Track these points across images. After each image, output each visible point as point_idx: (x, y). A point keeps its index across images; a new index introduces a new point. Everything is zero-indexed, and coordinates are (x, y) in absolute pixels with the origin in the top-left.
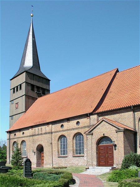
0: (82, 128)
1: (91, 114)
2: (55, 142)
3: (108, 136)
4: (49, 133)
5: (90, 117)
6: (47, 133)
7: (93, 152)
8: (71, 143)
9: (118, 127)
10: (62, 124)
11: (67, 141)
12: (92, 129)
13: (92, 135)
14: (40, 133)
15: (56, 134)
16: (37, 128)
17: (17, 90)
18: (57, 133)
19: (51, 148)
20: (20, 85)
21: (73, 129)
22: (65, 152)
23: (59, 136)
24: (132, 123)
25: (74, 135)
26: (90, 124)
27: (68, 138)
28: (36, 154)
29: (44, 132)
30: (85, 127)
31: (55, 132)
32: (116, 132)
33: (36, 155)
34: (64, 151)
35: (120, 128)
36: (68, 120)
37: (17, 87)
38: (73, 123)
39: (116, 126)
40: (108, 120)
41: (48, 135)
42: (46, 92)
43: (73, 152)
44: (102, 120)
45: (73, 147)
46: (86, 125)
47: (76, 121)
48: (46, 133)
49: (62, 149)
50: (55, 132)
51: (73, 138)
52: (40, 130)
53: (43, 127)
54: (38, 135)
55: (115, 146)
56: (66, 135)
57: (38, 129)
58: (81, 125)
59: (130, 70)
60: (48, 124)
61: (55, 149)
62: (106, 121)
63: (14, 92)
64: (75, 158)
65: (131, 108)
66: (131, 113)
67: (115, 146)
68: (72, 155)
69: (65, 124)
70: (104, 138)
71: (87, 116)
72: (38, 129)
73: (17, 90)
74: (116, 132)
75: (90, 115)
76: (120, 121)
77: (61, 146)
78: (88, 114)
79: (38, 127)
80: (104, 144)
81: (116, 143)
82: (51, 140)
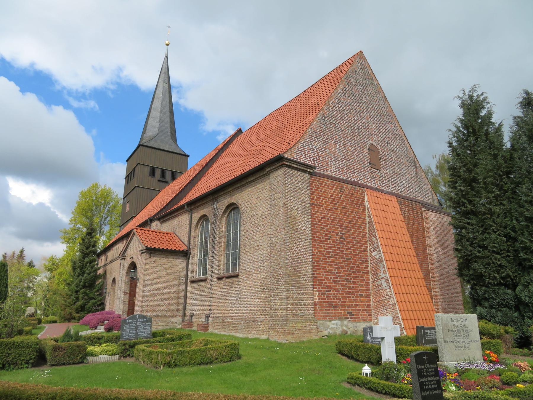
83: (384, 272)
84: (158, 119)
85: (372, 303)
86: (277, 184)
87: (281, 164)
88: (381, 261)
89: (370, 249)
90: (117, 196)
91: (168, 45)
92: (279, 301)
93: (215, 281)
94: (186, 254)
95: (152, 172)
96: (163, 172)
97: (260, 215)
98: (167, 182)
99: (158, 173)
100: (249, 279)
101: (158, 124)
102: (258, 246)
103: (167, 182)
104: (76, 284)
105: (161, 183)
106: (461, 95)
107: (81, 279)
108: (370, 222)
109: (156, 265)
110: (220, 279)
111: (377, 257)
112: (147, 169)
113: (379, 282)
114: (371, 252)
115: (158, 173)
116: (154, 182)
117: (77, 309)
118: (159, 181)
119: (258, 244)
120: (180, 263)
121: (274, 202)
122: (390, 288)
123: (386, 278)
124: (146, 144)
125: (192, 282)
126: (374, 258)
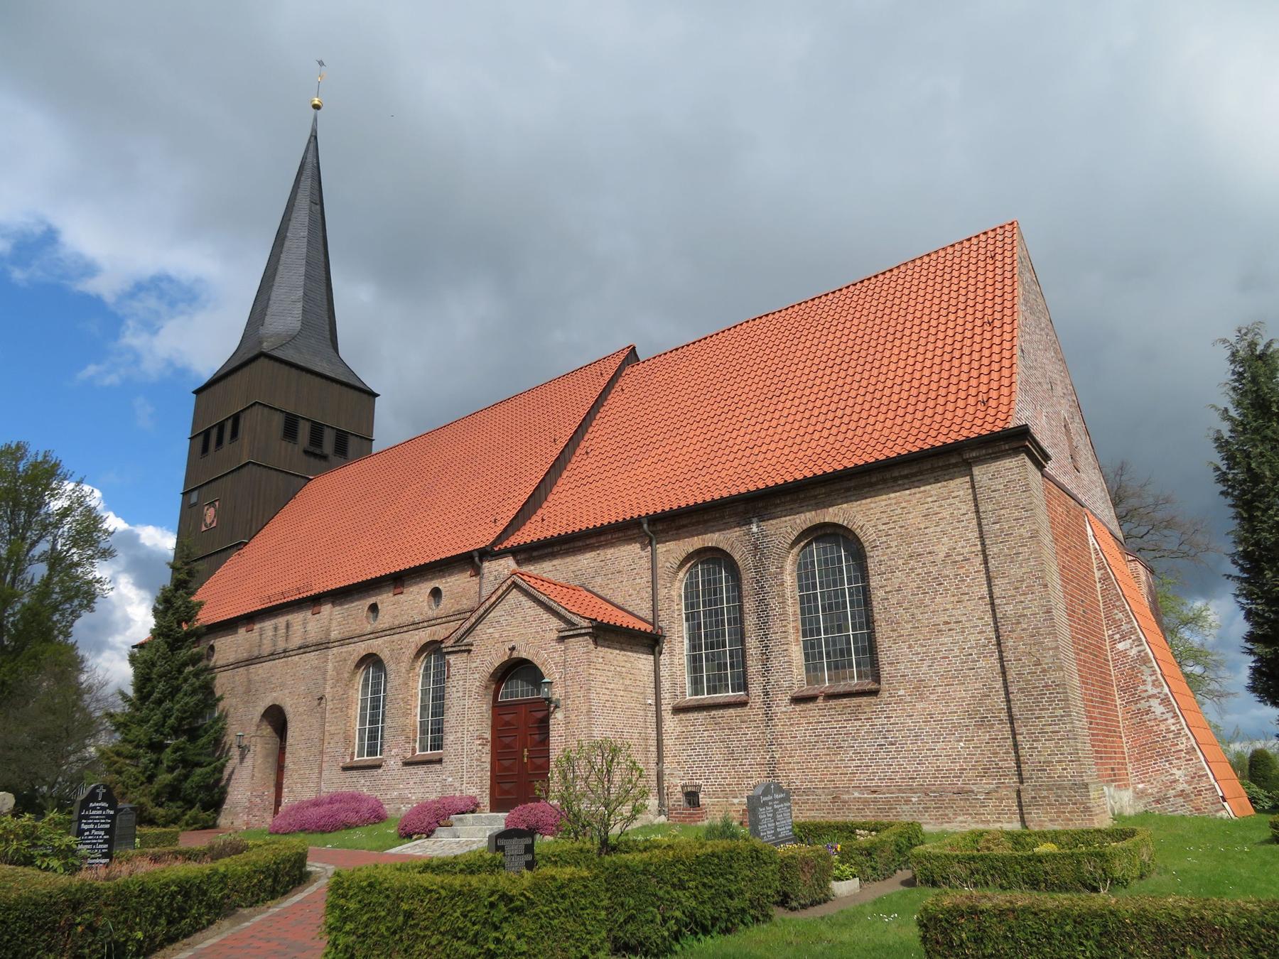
1: (487, 553)
9: (569, 616)
10: (372, 600)
12: (467, 625)
14: (281, 645)
15: (344, 649)
16: (268, 625)
20: (236, 418)
21: (415, 626)
22: (433, 739)
23: (356, 657)
24: (647, 594)
25: (357, 659)
27: (391, 666)
29: (296, 641)
31: (343, 641)
34: (373, 736)
35: (576, 619)
36: (398, 580)
37: (221, 426)
38: (416, 598)
39: (563, 612)
40: (533, 581)
42: (353, 443)
44: (509, 582)
46: (466, 604)
47: (426, 587)
48: (304, 648)
50: (343, 641)
52: (282, 631)
53: (296, 619)
54: (273, 656)
56: (385, 655)
58: (447, 604)
59: (764, 319)
60: (315, 601)
62: (525, 585)
63: (205, 449)
64: (421, 770)
69: (386, 600)
71: (470, 561)
72: (276, 629)
73: (220, 442)
75: (481, 561)
76: (598, 584)
79: (276, 616)
80: (518, 691)
83: (1155, 683)
84: (301, 293)
85: (1126, 750)
86: (1001, 487)
87: (1015, 445)
88: (1145, 660)
89: (1111, 637)
90: (1233, 506)
91: (317, 107)
92: (1051, 744)
93: (782, 706)
94: (651, 642)
95: (291, 427)
96: (317, 431)
97: (942, 555)
98: (324, 457)
99: (304, 431)
100: (921, 698)
101: (300, 305)
102: (946, 623)
103: (324, 457)
104: (156, 724)
105: (312, 459)
106: (1233, 339)
107: (170, 710)
108: (1106, 578)
109: (606, 667)
110: (797, 700)
111: (1134, 652)
112: (278, 421)
113: (1143, 705)
114: (1114, 642)
115: (304, 431)
116: (291, 454)
117: (158, 795)
118: (306, 452)
119: (947, 619)
120: (642, 662)
121: (998, 526)
122: (1175, 716)
123: (1162, 696)
124: (275, 353)
125: (677, 710)
126: (1124, 654)
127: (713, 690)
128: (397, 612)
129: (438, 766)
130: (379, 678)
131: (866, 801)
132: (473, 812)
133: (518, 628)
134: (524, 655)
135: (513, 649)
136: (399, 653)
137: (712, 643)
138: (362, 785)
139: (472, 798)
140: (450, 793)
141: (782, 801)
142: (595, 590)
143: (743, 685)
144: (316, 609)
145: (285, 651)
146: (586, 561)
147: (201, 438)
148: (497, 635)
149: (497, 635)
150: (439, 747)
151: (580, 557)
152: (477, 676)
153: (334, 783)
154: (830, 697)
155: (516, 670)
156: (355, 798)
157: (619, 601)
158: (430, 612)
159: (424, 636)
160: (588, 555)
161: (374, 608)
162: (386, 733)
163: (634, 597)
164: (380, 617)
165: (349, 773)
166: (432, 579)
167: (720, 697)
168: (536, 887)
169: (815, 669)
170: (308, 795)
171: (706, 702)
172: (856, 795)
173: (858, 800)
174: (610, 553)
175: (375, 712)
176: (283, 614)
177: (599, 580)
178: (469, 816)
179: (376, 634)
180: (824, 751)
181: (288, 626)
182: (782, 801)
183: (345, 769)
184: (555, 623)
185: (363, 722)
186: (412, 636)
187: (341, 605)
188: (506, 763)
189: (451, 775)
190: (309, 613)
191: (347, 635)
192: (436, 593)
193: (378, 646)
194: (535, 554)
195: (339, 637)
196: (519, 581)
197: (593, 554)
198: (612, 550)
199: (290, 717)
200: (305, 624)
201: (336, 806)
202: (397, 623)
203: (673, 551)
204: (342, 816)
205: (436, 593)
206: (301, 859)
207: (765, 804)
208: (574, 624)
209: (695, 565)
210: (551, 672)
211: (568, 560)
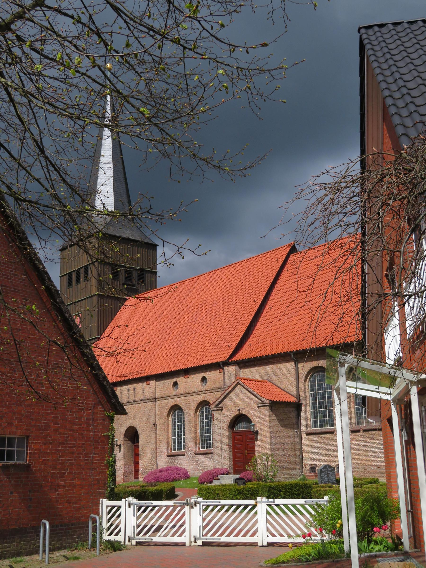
0: (211, 391)
1: (226, 363)
2: (161, 421)
3: (246, 414)
4: (150, 400)
5: (223, 369)
6: (145, 400)
7: (223, 446)
8: (192, 421)
9: (261, 398)
10: (175, 380)
11: (184, 418)
13: (222, 410)
14: (132, 399)
15: (163, 402)
17: (78, 281)
18: (166, 401)
19: (153, 436)
21: (196, 393)
24: (294, 385)
25: (170, 407)
26: (224, 385)
27: (186, 411)
28: (122, 449)
29: (139, 397)
30: (215, 390)
31: (163, 398)
32: (259, 407)
33: (122, 452)
34: (180, 441)
35: (264, 400)
36: (186, 372)
37: (78, 272)
39: (258, 396)
41: (148, 405)
43: (196, 443)
44: (236, 382)
45: (195, 433)
46: (218, 385)
47: (200, 376)
48: (143, 401)
49: (16, 449)
50: (163, 398)
51: (196, 412)
52: (132, 392)
53: (139, 386)
55: (257, 432)
56: (183, 406)
57: (128, 390)
58: (209, 384)
60: (147, 379)
61: (162, 437)
63: (70, 284)
64: (203, 457)
65: (290, 355)
66: (291, 365)
67: (257, 432)
68: (193, 449)
69: (181, 380)
70: (240, 418)
72: (128, 390)
73: (78, 281)
74: (259, 407)
75: (224, 366)
76: (274, 379)
77: (174, 429)
78: (221, 363)
80: (241, 427)
81: (257, 428)
82: (153, 416)
96: (129, 272)
125: (308, 434)
127: (322, 426)
128: (187, 387)
129: (210, 455)
130: (180, 415)
131: (376, 471)
132: (227, 474)
133: (241, 401)
134: (244, 413)
135: (239, 410)
136: (189, 405)
137: (321, 406)
138: (176, 462)
139: (226, 469)
140: (217, 467)
141: (331, 471)
142: (273, 382)
143: (332, 424)
144: (148, 382)
145: (134, 401)
146: (269, 369)
147: (66, 277)
148: (232, 404)
149: (232, 404)
150: (210, 447)
151: (266, 367)
152: (225, 420)
153: (164, 462)
154: (365, 431)
155: (240, 418)
156: (177, 469)
157: (283, 387)
158: (202, 388)
159: (200, 398)
160: (270, 366)
161: (175, 384)
162: (186, 440)
163: (289, 386)
164: (179, 388)
165: (170, 458)
166: (202, 372)
167: (324, 429)
168: (244, 488)
169: (360, 418)
170: (152, 468)
171: (318, 431)
172: (373, 468)
173: (373, 470)
174: (279, 366)
175: (179, 431)
176: (131, 384)
177: (275, 377)
178: (225, 476)
179: (178, 396)
180: (362, 452)
181: (134, 390)
182: (331, 471)
183: (168, 456)
184: (256, 400)
185: (174, 436)
186: (195, 398)
187: (160, 381)
188: (239, 455)
189: (217, 460)
190: (144, 384)
191: (164, 395)
192: (204, 379)
193: (180, 401)
194: (247, 364)
195: (160, 396)
196: (240, 382)
197: (272, 366)
198: (280, 365)
199: (140, 432)
200: (143, 388)
201: (170, 472)
202: (187, 391)
203: (305, 367)
204: (173, 476)
205: (204, 379)
206: (173, 489)
207: (324, 472)
208: (263, 402)
209: (312, 376)
210: (255, 420)
211: (261, 367)
